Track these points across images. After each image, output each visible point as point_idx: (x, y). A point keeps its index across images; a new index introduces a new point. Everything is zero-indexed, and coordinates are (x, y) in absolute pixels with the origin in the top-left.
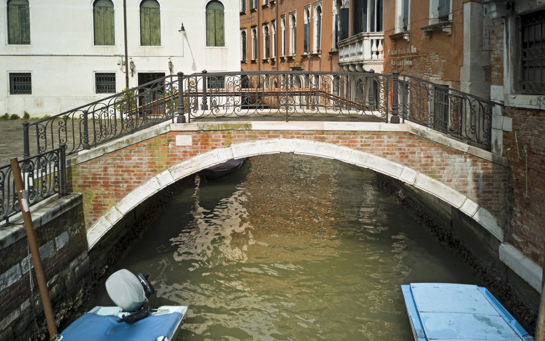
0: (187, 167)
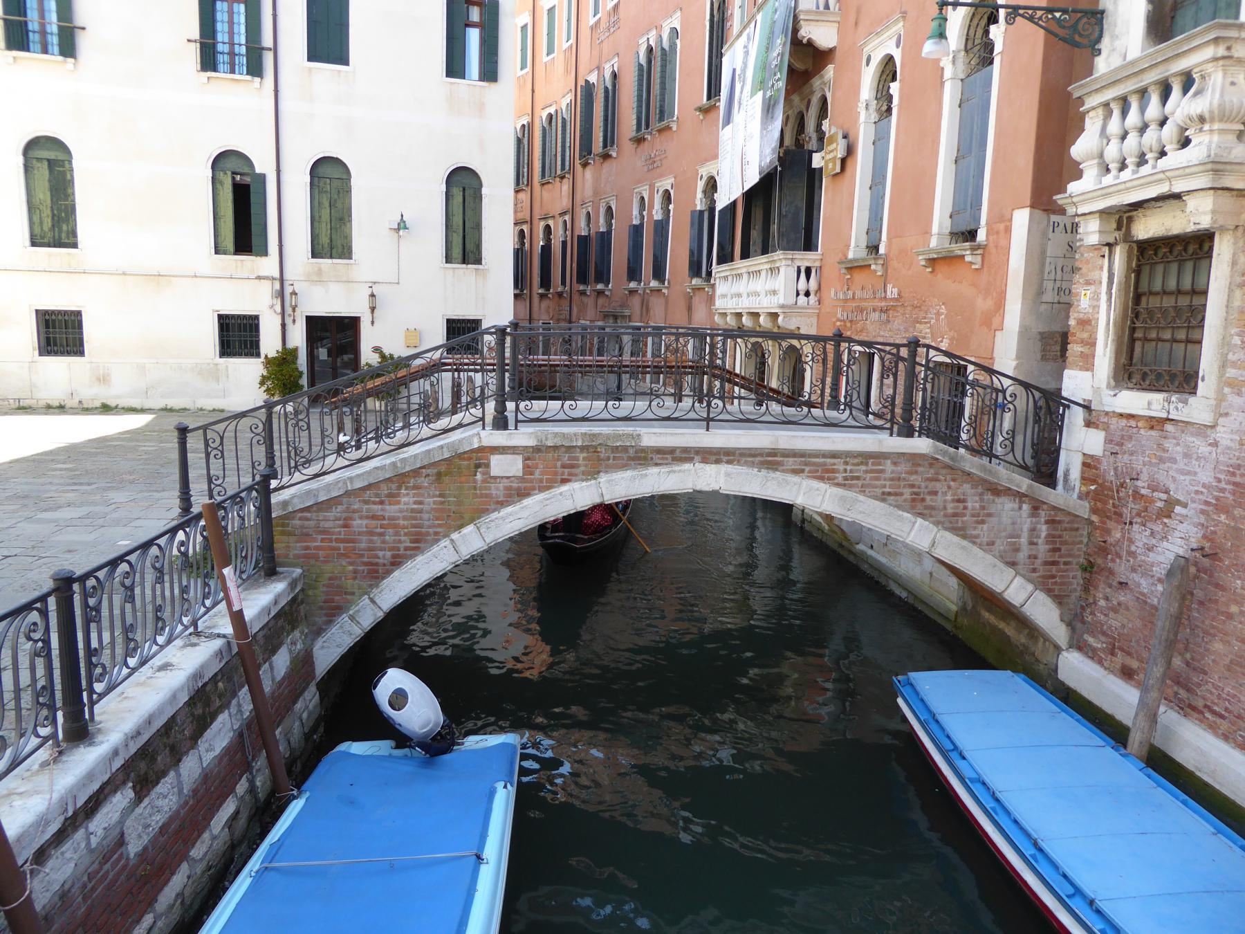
0: (511, 518)
